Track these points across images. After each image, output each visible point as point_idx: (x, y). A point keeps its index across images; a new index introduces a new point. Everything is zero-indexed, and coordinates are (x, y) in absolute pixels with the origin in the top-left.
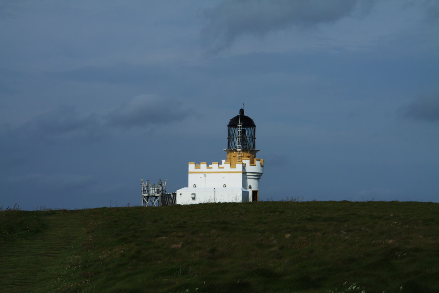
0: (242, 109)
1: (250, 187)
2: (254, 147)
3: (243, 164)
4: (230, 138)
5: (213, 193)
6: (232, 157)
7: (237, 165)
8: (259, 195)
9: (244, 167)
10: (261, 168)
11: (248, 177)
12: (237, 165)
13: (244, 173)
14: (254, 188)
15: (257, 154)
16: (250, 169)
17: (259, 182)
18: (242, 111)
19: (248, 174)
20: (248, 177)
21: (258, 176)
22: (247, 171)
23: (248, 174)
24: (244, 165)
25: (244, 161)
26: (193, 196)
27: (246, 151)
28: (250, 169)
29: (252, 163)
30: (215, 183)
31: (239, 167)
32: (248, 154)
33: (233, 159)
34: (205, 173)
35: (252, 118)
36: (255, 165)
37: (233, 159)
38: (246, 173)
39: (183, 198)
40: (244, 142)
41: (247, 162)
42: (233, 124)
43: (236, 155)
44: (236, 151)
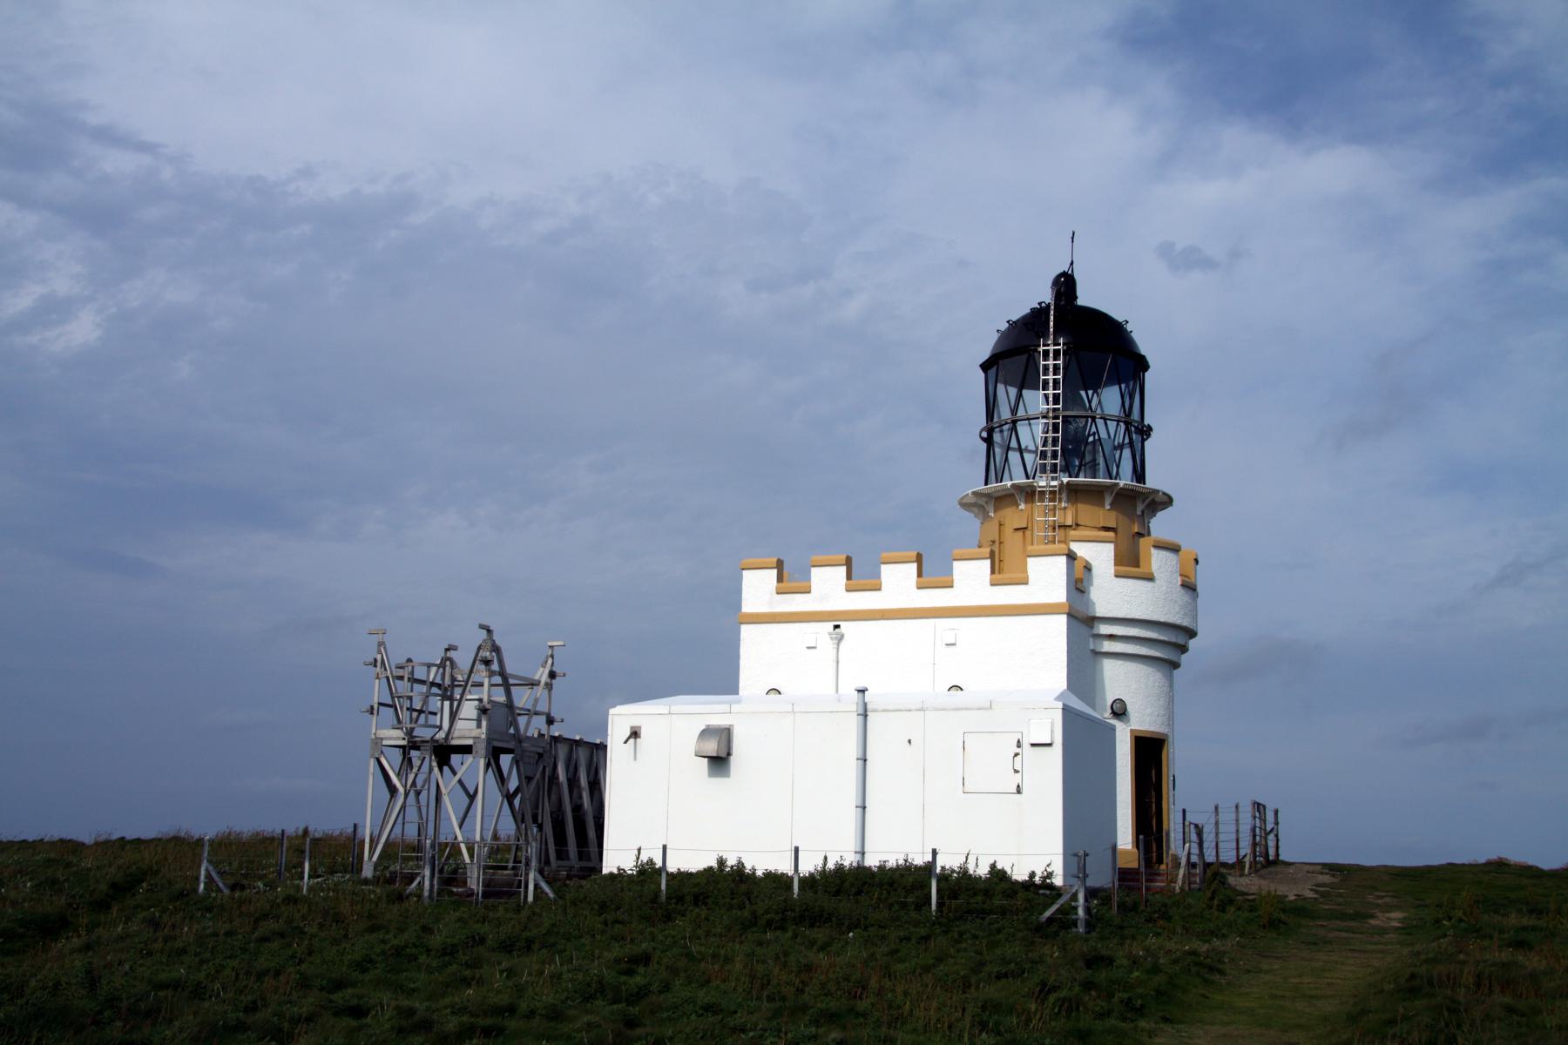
0: (1064, 274)
1: (1120, 711)
2: (1139, 475)
3: (1071, 556)
4: (996, 433)
5: (854, 722)
6: (1008, 530)
7: (1032, 563)
8: (1179, 762)
9: (1079, 581)
10: (1181, 596)
11: (1108, 646)
12: (1032, 563)
13: (1082, 620)
14: (1144, 719)
15: (1161, 526)
16: (1112, 595)
17: (1171, 685)
18: (1065, 285)
19: (1105, 629)
20: (1108, 646)
21: (1170, 645)
22: (1100, 611)
23: (1105, 629)
24: (1078, 565)
25: (1080, 549)
26: (712, 747)
27: (1093, 494)
28: (1112, 595)
29: (1130, 563)
30: (884, 721)
31: (1047, 577)
32: (1104, 514)
33: (1013, 541)
34: (836, 619)
35: (1119, 318)
36: (1150, 578)
37: (1013, 541)
38: (1092, 621)
39: (660, 815)
40: (1073, 447)
41: (1099, 555)
42: (1012, 358)
43: (1031, 518)
44: (1030, 493)
